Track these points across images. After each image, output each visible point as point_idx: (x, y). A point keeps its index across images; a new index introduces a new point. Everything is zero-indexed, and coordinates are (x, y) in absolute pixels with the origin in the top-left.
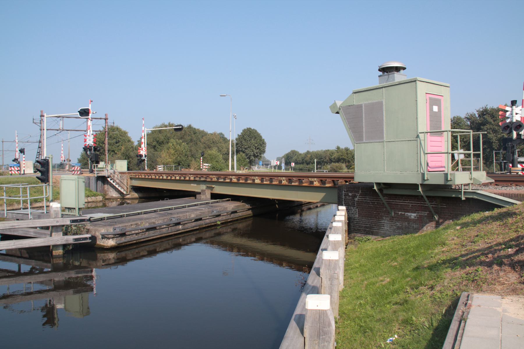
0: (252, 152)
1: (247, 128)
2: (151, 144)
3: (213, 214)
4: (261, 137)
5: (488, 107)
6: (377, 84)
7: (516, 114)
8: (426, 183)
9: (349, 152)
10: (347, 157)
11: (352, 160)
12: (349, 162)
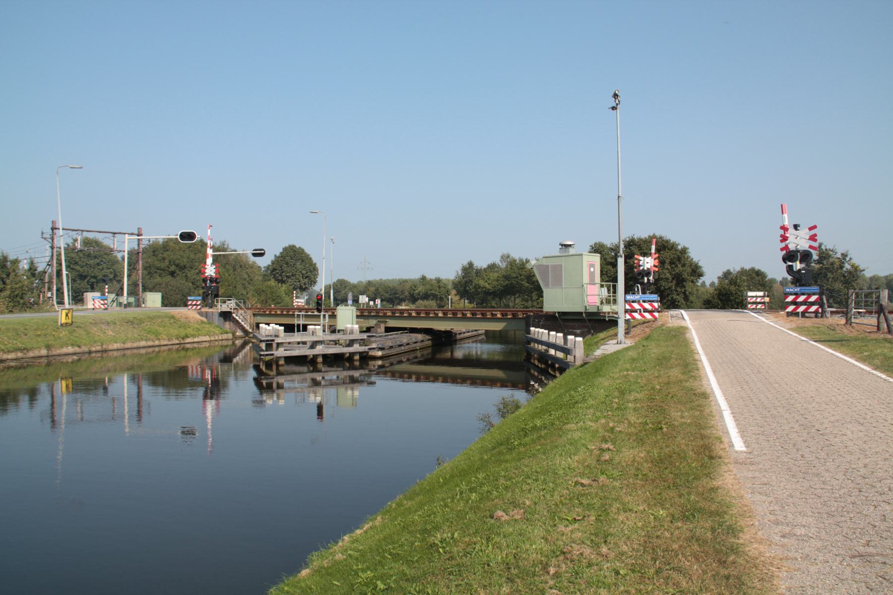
0: (298, 283)
1: (290, 246)
2: (167, 269)
3: (397, 344)
4: (311, 259)
5: (635, 237)
6: (559, 254)
7: (647, 263)
8: (587, 311)
9: (442, 285)
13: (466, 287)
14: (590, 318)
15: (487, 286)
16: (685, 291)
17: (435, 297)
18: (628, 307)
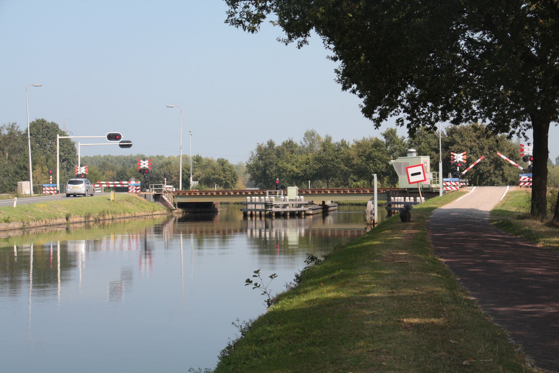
7: (459, 157)
9: (227, 167)
10: (224, 177)
11: (232, 182)
13: (265, 170)
14: (425, 191)
15: (296, 169)
16: (503, 173)
17: (219, 182)
18: (444, 184)
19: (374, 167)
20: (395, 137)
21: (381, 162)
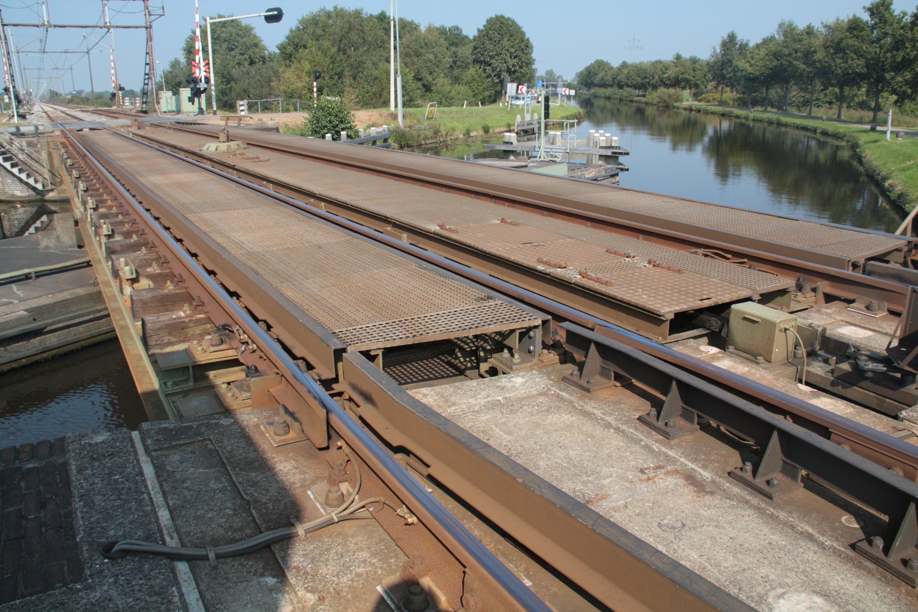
1: (497, 17)
12: (696, 86)
15: (748, 68)
19: (842, 65)
20: (889, 12)
21: (856, 55)
